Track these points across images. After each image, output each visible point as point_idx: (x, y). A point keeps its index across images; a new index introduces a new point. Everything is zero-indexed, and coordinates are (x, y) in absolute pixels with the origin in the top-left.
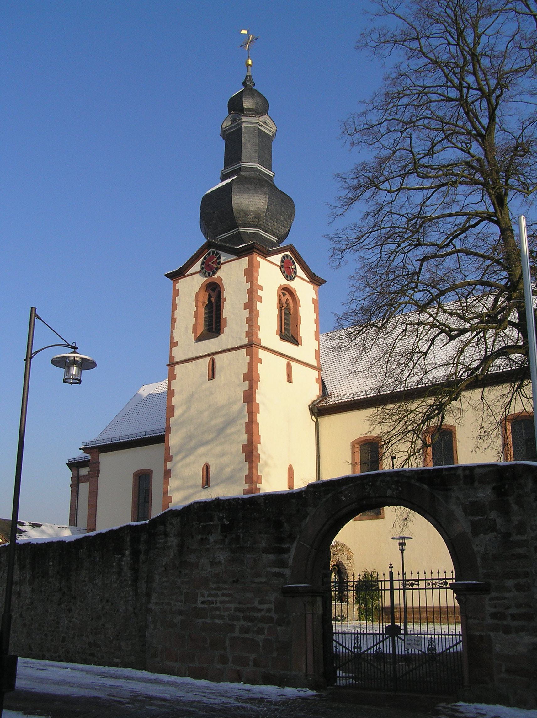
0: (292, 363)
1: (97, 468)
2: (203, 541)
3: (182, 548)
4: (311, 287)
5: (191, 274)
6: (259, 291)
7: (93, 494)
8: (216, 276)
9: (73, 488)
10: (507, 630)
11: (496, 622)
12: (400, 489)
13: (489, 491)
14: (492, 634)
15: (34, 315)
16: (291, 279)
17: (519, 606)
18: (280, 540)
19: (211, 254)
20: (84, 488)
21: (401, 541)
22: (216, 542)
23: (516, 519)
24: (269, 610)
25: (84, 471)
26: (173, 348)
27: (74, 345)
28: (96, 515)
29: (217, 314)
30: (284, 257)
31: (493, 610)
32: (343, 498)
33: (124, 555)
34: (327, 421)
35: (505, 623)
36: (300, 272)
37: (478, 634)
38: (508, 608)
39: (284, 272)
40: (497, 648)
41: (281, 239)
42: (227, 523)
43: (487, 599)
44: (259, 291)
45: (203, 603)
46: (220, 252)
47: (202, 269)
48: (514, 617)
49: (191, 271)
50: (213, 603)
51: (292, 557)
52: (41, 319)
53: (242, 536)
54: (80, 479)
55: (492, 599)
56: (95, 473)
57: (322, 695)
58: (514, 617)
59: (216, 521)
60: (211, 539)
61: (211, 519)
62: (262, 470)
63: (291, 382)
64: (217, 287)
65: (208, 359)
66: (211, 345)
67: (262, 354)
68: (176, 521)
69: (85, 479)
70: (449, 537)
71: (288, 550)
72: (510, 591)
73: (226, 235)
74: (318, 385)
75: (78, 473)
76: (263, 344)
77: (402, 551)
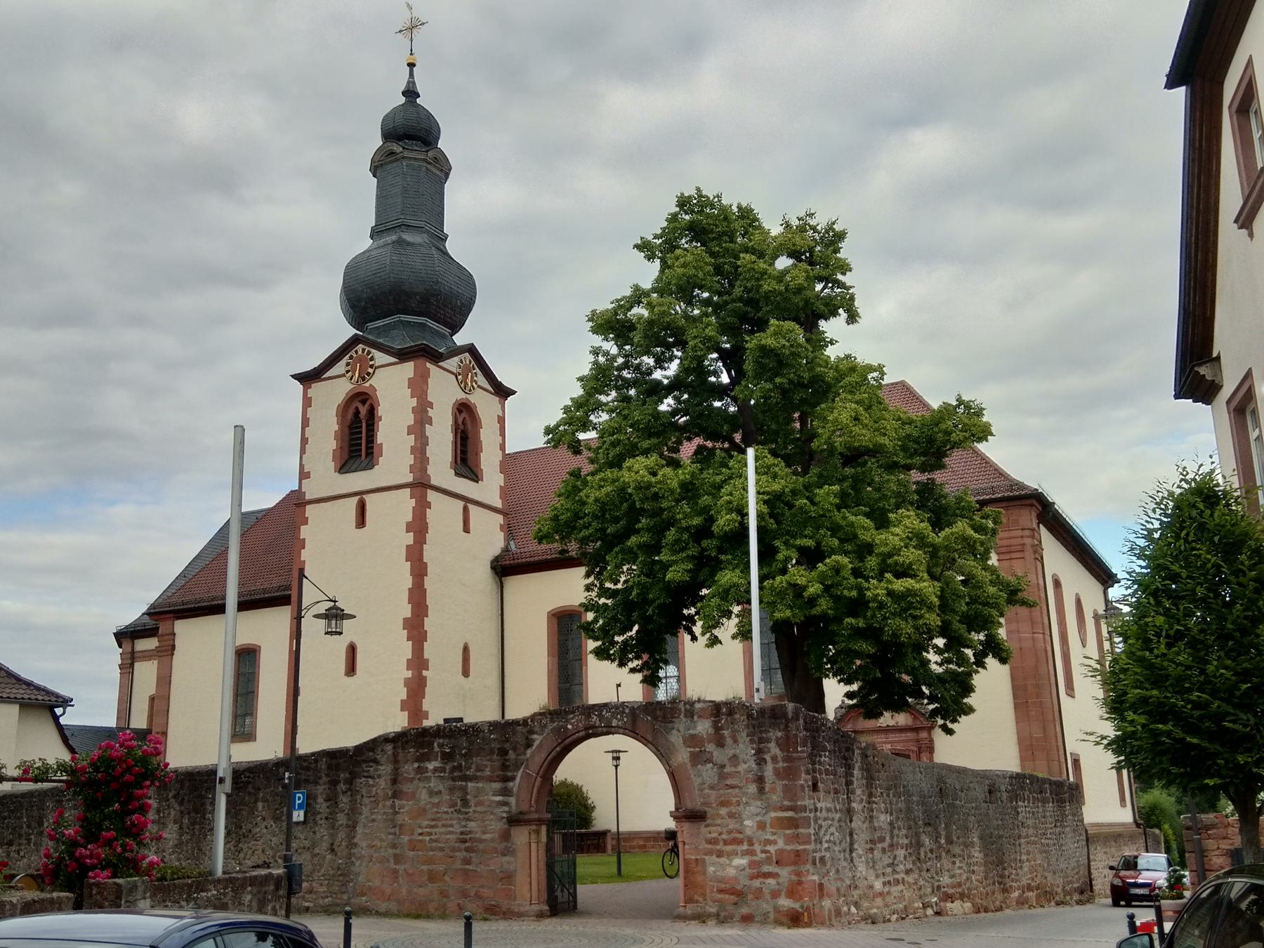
0: (471, 507)
1: (171, 642)
5: (330, 378)
8: (367, 385)
9: (123, 671)
10: (720, 854)
12: (625, 720)
17: (730, 832)
19: (360, 352)
20: (146, 673)
21: (615, 755)
23: (730, 752)
24: (492, 840)
25: (146, 644)
26: (303, 481)
29: (368, 437)
32: (570, 727)
34: (518, 585)
35: (718, 847)
38: (720, 834)
40: (711, 869)
46: (373, 351)
50: (432, 834)
51: (517, 785)
53: (463, 763)
54: (136, 655)
55: (707, 826)
56: (167, 651)
57: (923, 471)
63: (468, 532)
64: (368, 399)
65: (355, 499)
66: (358, 480)
67: (432, 496)
68: (389, 747)
69: (147, 655)
70: (670, 767)
71: (513, 779)
72: (723, 818)
73: (379, 323)
75: (133, 647)
76: (434, 482)
77: (616, 767)
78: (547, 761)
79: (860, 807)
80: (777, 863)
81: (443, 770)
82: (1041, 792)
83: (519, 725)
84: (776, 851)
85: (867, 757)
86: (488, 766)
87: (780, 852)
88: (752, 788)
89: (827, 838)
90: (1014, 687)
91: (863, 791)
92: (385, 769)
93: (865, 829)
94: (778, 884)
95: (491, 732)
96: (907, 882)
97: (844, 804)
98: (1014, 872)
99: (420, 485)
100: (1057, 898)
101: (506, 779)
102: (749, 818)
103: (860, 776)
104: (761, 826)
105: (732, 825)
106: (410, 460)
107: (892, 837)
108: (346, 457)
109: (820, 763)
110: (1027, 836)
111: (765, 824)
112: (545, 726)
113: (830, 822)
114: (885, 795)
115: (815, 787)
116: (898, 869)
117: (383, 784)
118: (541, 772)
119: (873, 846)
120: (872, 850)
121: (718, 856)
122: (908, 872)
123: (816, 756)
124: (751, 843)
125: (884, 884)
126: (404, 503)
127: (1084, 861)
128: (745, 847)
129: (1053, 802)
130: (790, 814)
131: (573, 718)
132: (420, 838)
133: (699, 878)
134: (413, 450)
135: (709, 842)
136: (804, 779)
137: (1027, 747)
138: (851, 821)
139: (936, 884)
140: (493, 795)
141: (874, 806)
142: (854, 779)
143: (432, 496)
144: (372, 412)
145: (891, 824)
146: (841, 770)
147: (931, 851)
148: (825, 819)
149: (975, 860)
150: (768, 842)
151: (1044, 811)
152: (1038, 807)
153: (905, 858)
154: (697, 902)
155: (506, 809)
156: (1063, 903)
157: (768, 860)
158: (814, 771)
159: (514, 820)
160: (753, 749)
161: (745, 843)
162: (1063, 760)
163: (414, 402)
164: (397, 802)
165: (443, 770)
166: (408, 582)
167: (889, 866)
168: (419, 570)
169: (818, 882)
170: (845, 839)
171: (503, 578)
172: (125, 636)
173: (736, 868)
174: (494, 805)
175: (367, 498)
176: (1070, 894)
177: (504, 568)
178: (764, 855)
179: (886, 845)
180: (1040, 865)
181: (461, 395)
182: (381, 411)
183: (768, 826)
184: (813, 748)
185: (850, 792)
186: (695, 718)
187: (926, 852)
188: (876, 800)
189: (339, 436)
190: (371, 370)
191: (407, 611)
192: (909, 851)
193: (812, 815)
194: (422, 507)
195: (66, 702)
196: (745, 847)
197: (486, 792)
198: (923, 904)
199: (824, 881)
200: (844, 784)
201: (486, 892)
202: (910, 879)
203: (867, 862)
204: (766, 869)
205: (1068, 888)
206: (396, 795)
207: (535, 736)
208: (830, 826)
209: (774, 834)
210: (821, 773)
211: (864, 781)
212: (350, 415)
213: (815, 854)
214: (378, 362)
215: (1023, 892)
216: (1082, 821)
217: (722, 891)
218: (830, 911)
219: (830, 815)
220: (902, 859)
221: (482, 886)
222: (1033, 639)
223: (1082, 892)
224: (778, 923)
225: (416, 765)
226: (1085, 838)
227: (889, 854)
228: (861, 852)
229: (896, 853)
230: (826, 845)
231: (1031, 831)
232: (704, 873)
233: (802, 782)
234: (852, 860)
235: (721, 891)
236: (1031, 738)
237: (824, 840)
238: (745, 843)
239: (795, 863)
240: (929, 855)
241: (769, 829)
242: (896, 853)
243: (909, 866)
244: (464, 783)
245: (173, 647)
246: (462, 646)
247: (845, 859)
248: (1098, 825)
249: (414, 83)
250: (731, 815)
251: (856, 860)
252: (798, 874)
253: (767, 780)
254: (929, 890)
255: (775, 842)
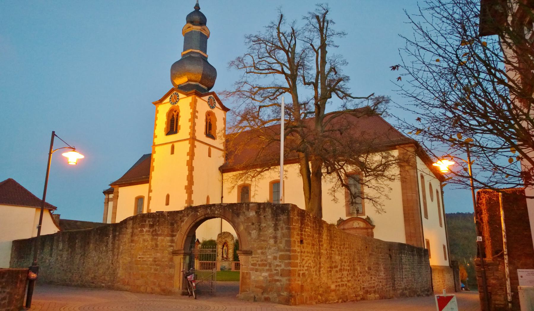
0: (212, 148)
2: (142, 231)
3: (133, 235)
4: (223, 112)
5: (165, 103)
6: (196, 113)
7: (115, 207)
8: (176, 105)
10: (257, 270)
11: (253, 267)
12: (221, 211)
13: (254, 213)
14: (251, 272)
15: (54, 134)
16: (213, 108)
17: (262, 261)
18: (173, 231)
22: (146, 231)
25: (111, 196)
27: (74, 148)
28: (116, 218)
30: (210, 97)
31: (252, 262)
32: (199, 214)
33: (109, 237)
35: (256, 267)
36: (217, 105)
37: (246, 272)
38: (257, 261)
39: (209, 105)
40: (253, 277)
41: (210, 88)
42: (151, 223)
43: (250, 258)
44: (196, 113)
45: (140, 258)
46: (179, 93)
47: (170, 101)
48: (259, 265)
49: (164, 102)
52: (57, 136)
53: (157, 229)
54: (109, 199)
55: (252, 258)
58: (259, 265)
59: (147, 222)
60: (145, 230)
61: (145, 222)
62: (193, 197)
66: (172, 138)
67: (196, 143)
68: (131, 222)
69: (112, 200)
72: (259, 254)
74: (224, 158)
76: (197, 138)
78: (189, 228)
79: (325, 252)
80: (281, 275)
81: (149, 231)
82: (412, 252)
83: (179, 213)
84: (281, 270)
85: (330, 230)
86: (166, 230)
87: (283, 270)
88: (272, 241)
89: (307, 265)
90: (404, 214)
91: (327, 245)
92: (129, 231)
93: (327, 262)
94: (281, 285)
95: (168, 216)
96: (348, 286)
97: (317, 250)
98: (399, 282)
99: (193, 139)
100: (418, 293)
101: (173, 236)
102: (270, 255)
103: (326, 239)
104: (275, 258)
105: (263, 257)
106: (189, 130)
107: (341, 266)
108: (169, 130)
109: (305, 231)
110: (406, 269)
111: (277, 257)
112: (189, 214)
113: (309, 258)
114: (338, 248)
115: (302, 242)
116: (344, 280)
117: (128, 236)
118: (187, 233)
119: (331, 270)
120: (331, 271)
121: (256, 271)
122: (348, 281)
123: (303, 228)
124: (270, 266)
125: (336, 286)
126: (186, 146)
127: (429, 279)
128: (267, 268)
129: (417, 256)
130: (288, 253)
131: (200, 210)
132: (140, 259)
133: (248, 281)
134: (190, 127)
135: (252, 265)
136: (296, 238)
137: (409, 235)
138: (320, 258)
139: (362, 287)
140: (168, 243)
141: (333, 252)
142: (323, 240)
143: (196, 143)
144: (178, 115)
145: (341, 260)
146: (316, 236)
147: (361, 273)
148: (306, 256)
149: (381, 277)
150: (277, 266)
151: (413, 259)
152: (411, 257)
153: (347, 275)
154: (247, 291)
155: (172, 248)
156: (420, 295)
157: (277, 274)
158: (301, 234)
159: (175, 253)
160: (273, 224)
161: (268, 266)
162: (422, 241)
163: (191, 111)
164: (132, 244)
165: (149, 231)
166: (187, 173)
167: (339, 278)
168: (191, 169)
169: (300, 284)
170: (317, 266)
171: (223, 174)
172: (107, 192)
173: (263, 277)
174: (168, 246)
175: (175, 144)
176: (423, 292)
177: (223, 170)
178: (275, 272)
179: (338, 269)
180: (411, 280)
181: (209, 109)
182: (180, 114)
183: (278, 258)
184: (302, 224)
185: (320, 246)
186: (250, 210)
187: (358, 273)
188: (334, 250)
189: (167, 123)
190: (177, 100)
191: (186, 183)
192: (350, 272)
193: (299, 254)
194: (193, 147)
195: (55, 208)
196: (267, 268)
197: (164, 240)
198: (355, 295)
199: (305, 284)
200: (317, 242)
201: (163, 283)
202: (350, 284)
203: (328, 277)
204: (277, 278)
205: (423, 289)
206: (132, 241)
207: (185, 218)
208: (308, 260)
209: (280, 262)
210: (305, 236)
211: (328, 241)
212: (171, 115)
213: (299, 272)
214: (180, 97)
215: (403, 291)
216: (429, 264)
217: (257, 287)
218: (306, 298)
219: (309, 254)
220: (346, 275)
221: (161, 281)
222: (412, 196)
223: (428, 291)
224: (280, 303)
225: (140, 229)
226: (430, 270)
227: (340, 273)
228: (324, 272)
229: (343, 273)
230: (306, 268)
231: (408, 266)
232: (250, 278)
233: (294, 239)
234: (320, 275)
235: (256, 287)
236: (410, 232)
237: (305, 266)
238: (268, 266)
239: (289, 275)
240: (360, 274)
241: (278, 260)
242: (343, 273)
243: (349, 279)
244: (157, 237)
245: (118, 196)
246: (207, 196)
247: (316, 275)
248: (433, 266)
249: (198, 4)
250: (262, 253)
251: (322, 275)
252: (289, 280)
253: (278, 238)
254: (359, 289)
255: (280, 266)
